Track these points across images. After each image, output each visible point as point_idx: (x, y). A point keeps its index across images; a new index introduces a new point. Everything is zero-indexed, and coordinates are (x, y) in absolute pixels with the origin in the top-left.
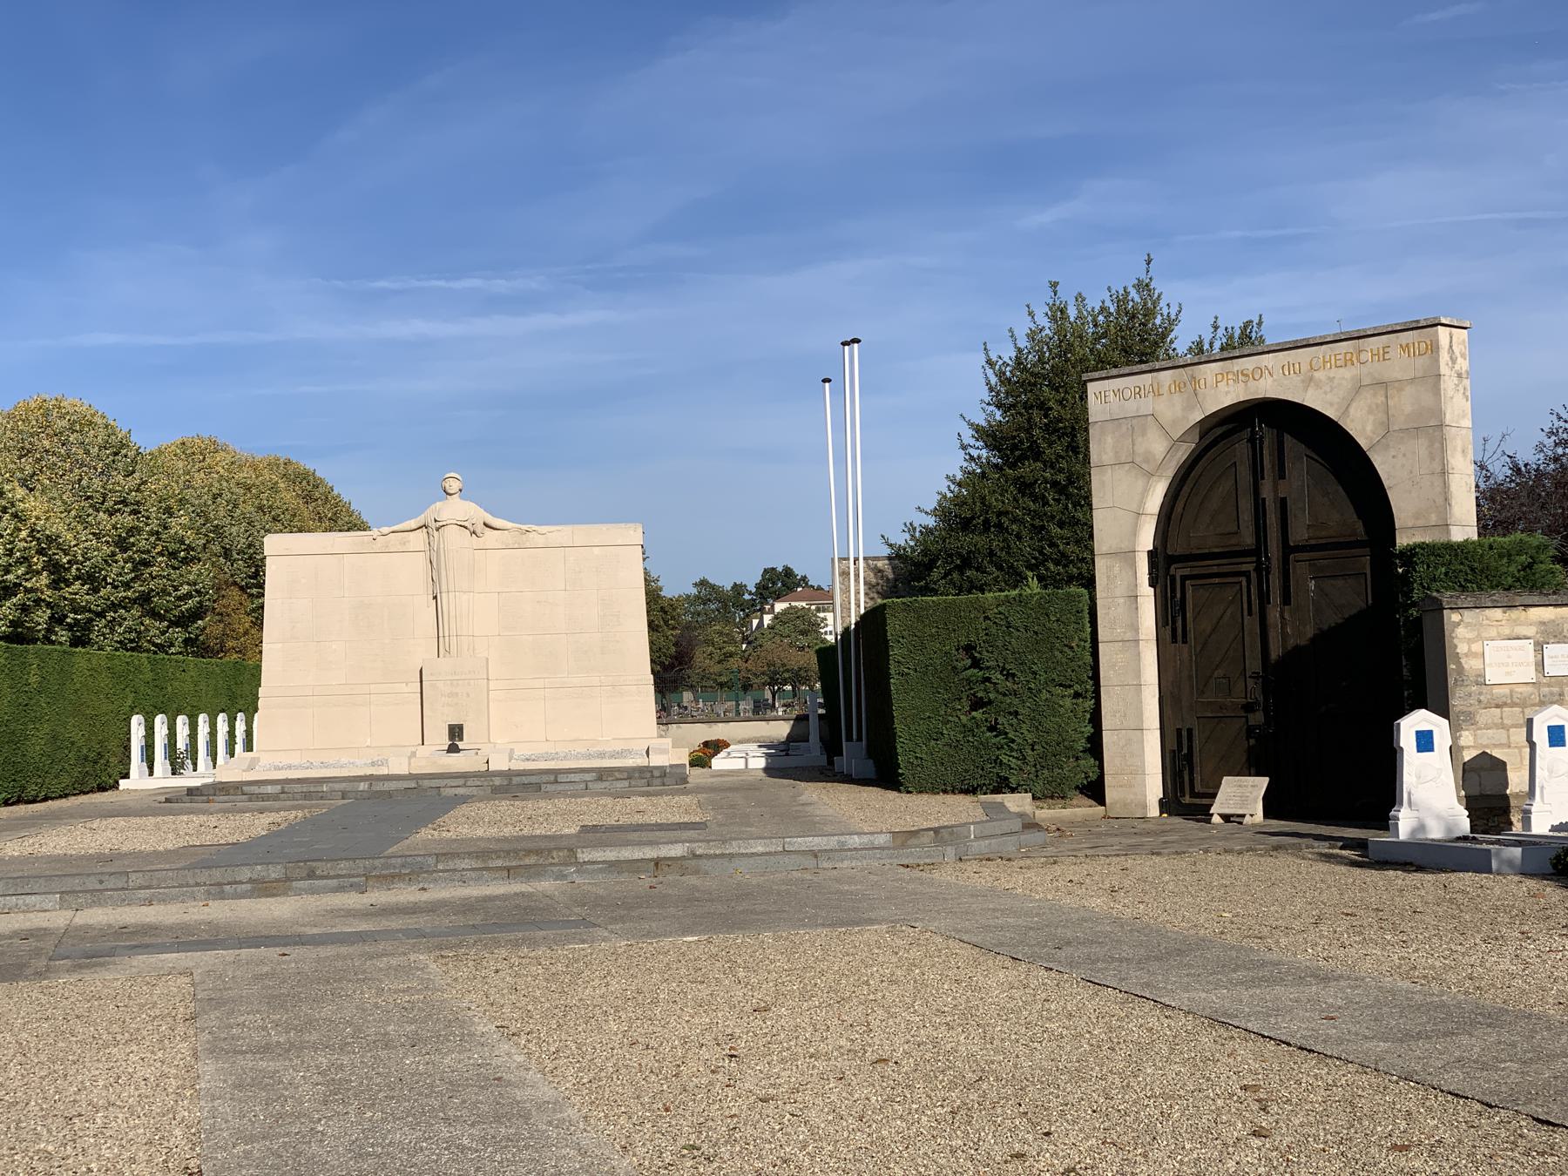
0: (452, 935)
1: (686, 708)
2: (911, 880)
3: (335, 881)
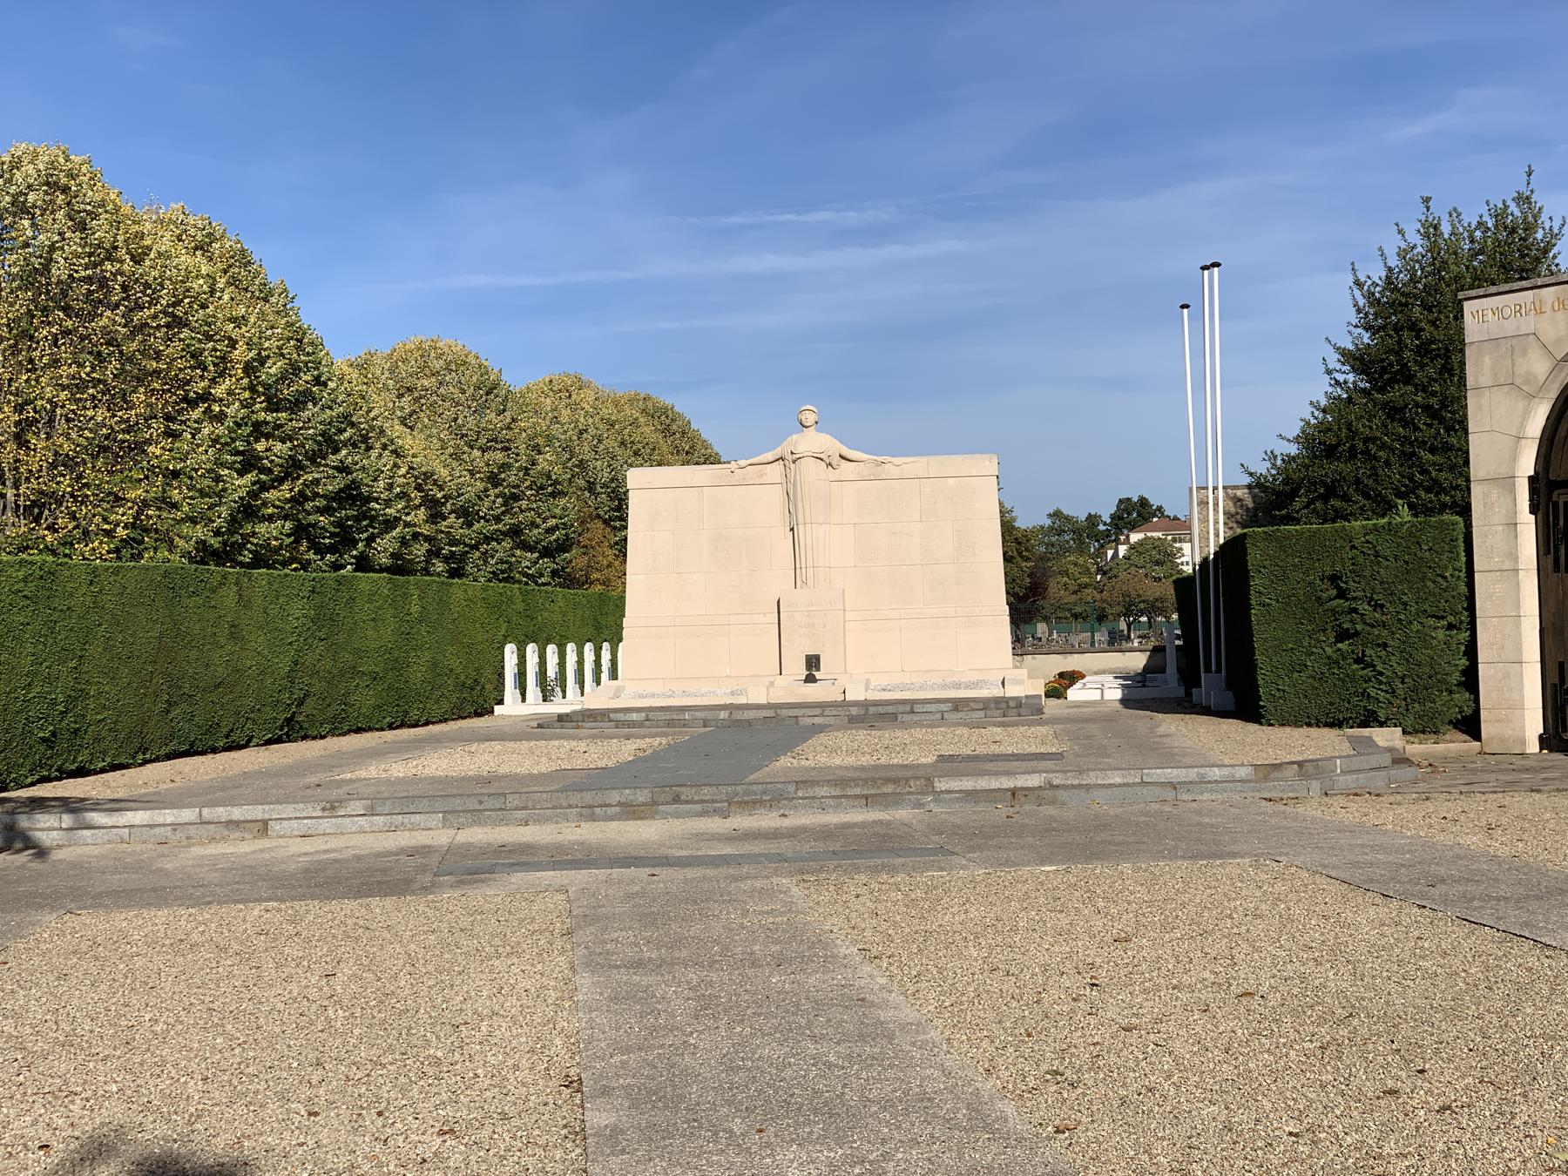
1: (1040, 639)
3: (699, 806)
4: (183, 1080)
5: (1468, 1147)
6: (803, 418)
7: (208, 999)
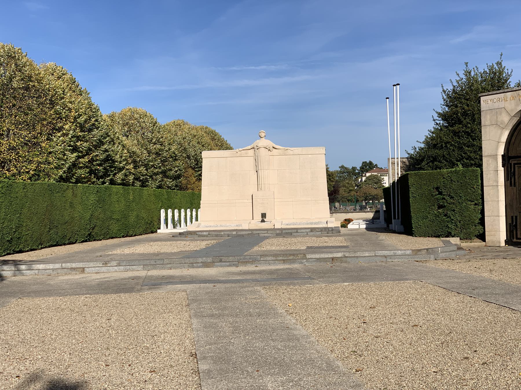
0: (267, 281)
1: (337, 208)
2: (419, 266)
3: (228, 263)
4: (63, 354)
5: (493, 376)
6: (261, 135)
7: (69, 327)
